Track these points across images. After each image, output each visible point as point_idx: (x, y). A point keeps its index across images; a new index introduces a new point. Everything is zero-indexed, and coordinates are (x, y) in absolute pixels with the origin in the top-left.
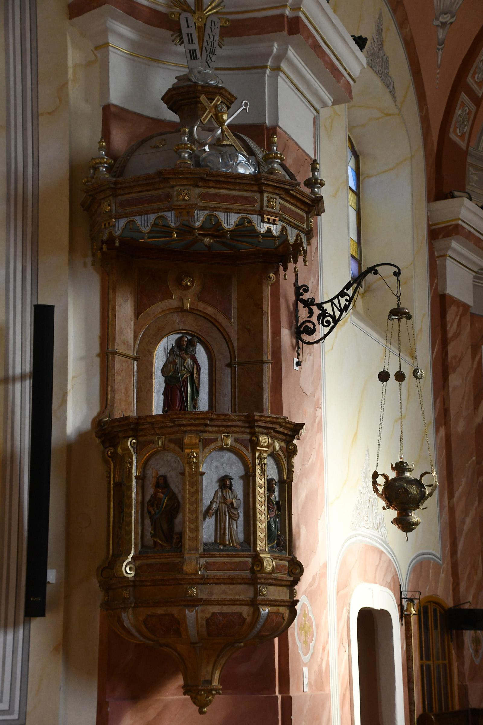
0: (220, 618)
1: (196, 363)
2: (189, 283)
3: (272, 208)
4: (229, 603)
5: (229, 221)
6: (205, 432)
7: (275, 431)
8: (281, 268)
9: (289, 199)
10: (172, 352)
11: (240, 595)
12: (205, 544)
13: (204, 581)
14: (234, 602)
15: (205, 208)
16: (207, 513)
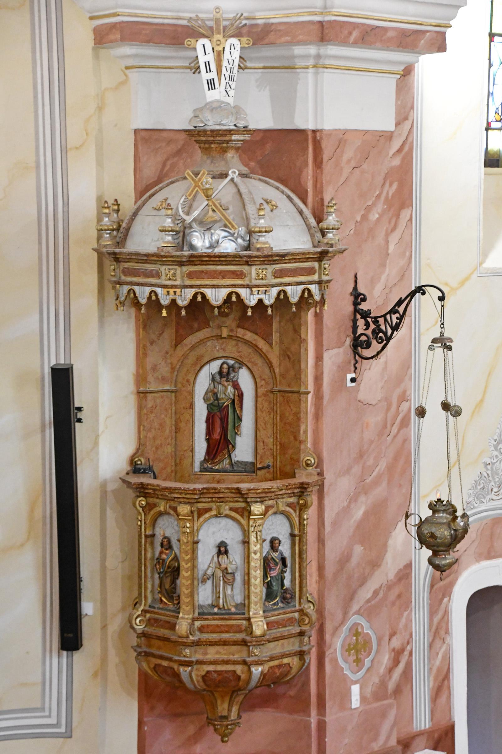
1: (237, 389)
2: (226, 310)
11: (233, 655)
12: (200, 607)
15: (191, 287)
16: (204, 581)
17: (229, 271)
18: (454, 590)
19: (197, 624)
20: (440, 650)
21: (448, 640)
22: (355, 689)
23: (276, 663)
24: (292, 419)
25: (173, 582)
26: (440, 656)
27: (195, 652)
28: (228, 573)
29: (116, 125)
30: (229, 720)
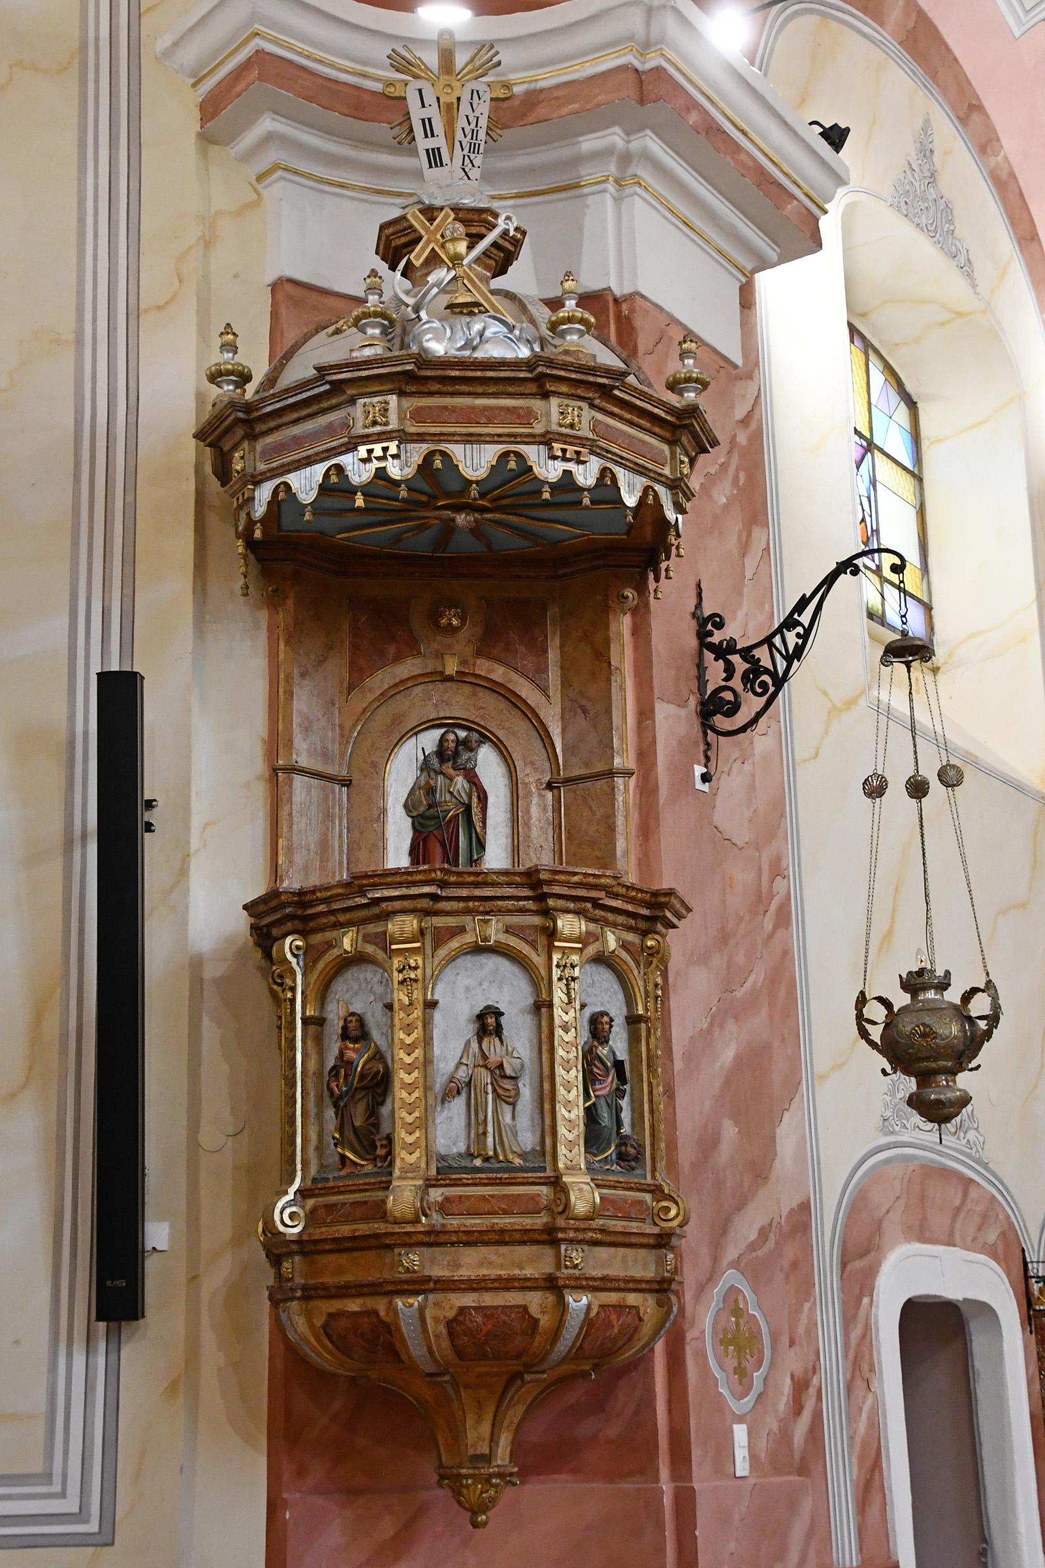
0: (479, 1319)
1: (475, 784)
2: (455, 622)
3: (572, 426)
4: (496, 1285)
5: (475, 462)
6: (437, 913)
7: (595, 903)
8: (651, 576)
9: (616, 410)
10: (425, 766)
11: (521, 1268)
12: (443, 1158)
13: (435, 1239)
14: (506, 1284)
16: (448, 1095)
17: (501, 408)
18: (877, 1284)
19: (436, 1194)
20: (864, 1403)
21: (875, 1385)
22: (740, 1433)
23: (612, 1298)
24: (597, 831)
26: (864, 1415)
27: (433, 1261)
29: (236, 276)
30: (494, 1464)
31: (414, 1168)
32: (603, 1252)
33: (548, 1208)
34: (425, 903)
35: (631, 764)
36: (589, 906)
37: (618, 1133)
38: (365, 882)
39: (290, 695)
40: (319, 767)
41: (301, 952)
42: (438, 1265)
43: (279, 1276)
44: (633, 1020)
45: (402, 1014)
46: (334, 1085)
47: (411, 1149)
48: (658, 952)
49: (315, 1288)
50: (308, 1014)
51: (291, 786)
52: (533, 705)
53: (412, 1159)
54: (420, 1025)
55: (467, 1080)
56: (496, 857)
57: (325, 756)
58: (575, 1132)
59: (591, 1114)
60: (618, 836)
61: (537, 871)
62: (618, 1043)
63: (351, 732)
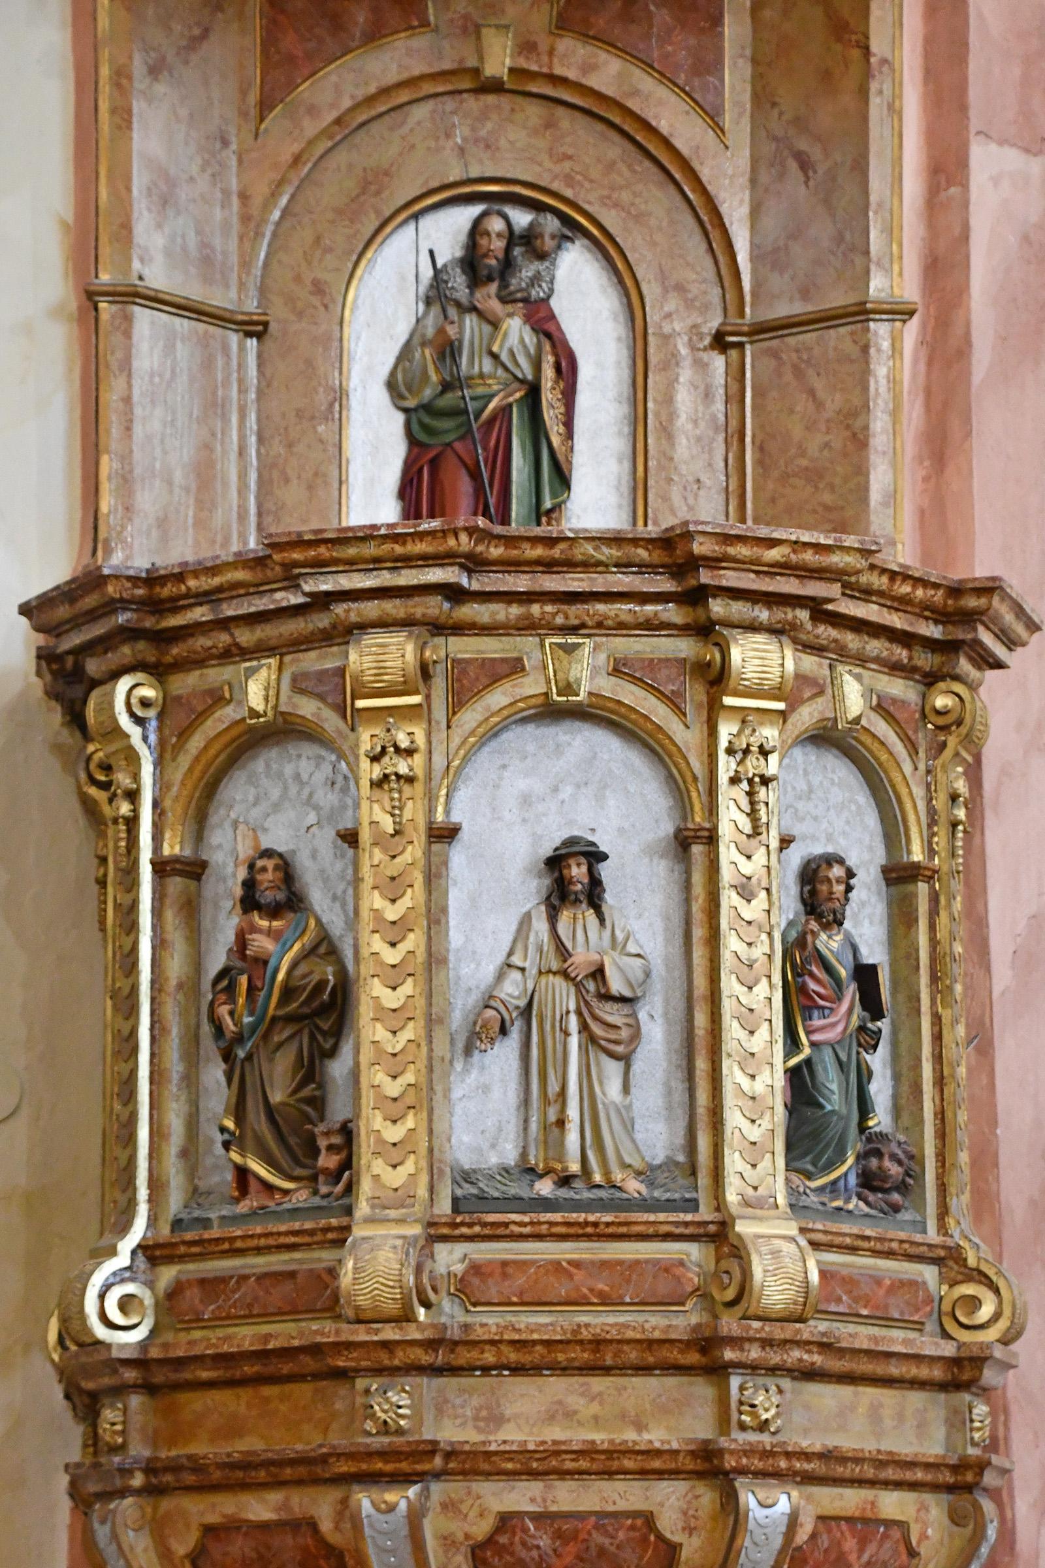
0: (544, 1542)
1: (548, 336)
4: (583, 1464)
6: (458, 629)
7: (819, 611)
10: (437, 293)
11: (640, 1427)
12: (467, 1177)
13: (446, 1358)
14: (605, 1463)
16: (483, 1032)
19: (450, 1258)
23: (849, 1500)
25: (310, 1072)
28: (607, 997)
31: (402, 1197)
32: (827, 1396)
33: (703, 1295)
34: (435, 606)
35: (909, 289)
36: (810, 614)
37: (862, 1128)
38: (296, 556)
39: (124, 117)
40: (195, 292)
41: (151, 713)
42: (445, 1415)
43: (93, 1441)
44: (899, 875)
45: (378, 855)
46: (223, 1011)
47: (395, 1155)
48: (959, 723)
49: (174, 1467)
50: (166, 851)
51: (128, 334)
52: (685, 151)
53: (396, 1178)
54: (418, 879)
55: (522, 1003)
56: (595, 501)
57: (207, 262)
58: (766, 1123)
59: (801, 1085)
60: (873, 458)
61: (688, 536)
62: (865, 928)
63: (267, 206)
